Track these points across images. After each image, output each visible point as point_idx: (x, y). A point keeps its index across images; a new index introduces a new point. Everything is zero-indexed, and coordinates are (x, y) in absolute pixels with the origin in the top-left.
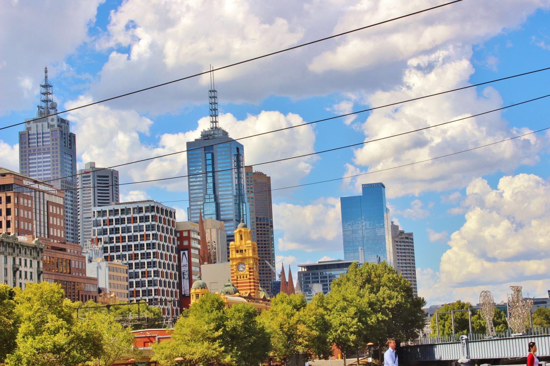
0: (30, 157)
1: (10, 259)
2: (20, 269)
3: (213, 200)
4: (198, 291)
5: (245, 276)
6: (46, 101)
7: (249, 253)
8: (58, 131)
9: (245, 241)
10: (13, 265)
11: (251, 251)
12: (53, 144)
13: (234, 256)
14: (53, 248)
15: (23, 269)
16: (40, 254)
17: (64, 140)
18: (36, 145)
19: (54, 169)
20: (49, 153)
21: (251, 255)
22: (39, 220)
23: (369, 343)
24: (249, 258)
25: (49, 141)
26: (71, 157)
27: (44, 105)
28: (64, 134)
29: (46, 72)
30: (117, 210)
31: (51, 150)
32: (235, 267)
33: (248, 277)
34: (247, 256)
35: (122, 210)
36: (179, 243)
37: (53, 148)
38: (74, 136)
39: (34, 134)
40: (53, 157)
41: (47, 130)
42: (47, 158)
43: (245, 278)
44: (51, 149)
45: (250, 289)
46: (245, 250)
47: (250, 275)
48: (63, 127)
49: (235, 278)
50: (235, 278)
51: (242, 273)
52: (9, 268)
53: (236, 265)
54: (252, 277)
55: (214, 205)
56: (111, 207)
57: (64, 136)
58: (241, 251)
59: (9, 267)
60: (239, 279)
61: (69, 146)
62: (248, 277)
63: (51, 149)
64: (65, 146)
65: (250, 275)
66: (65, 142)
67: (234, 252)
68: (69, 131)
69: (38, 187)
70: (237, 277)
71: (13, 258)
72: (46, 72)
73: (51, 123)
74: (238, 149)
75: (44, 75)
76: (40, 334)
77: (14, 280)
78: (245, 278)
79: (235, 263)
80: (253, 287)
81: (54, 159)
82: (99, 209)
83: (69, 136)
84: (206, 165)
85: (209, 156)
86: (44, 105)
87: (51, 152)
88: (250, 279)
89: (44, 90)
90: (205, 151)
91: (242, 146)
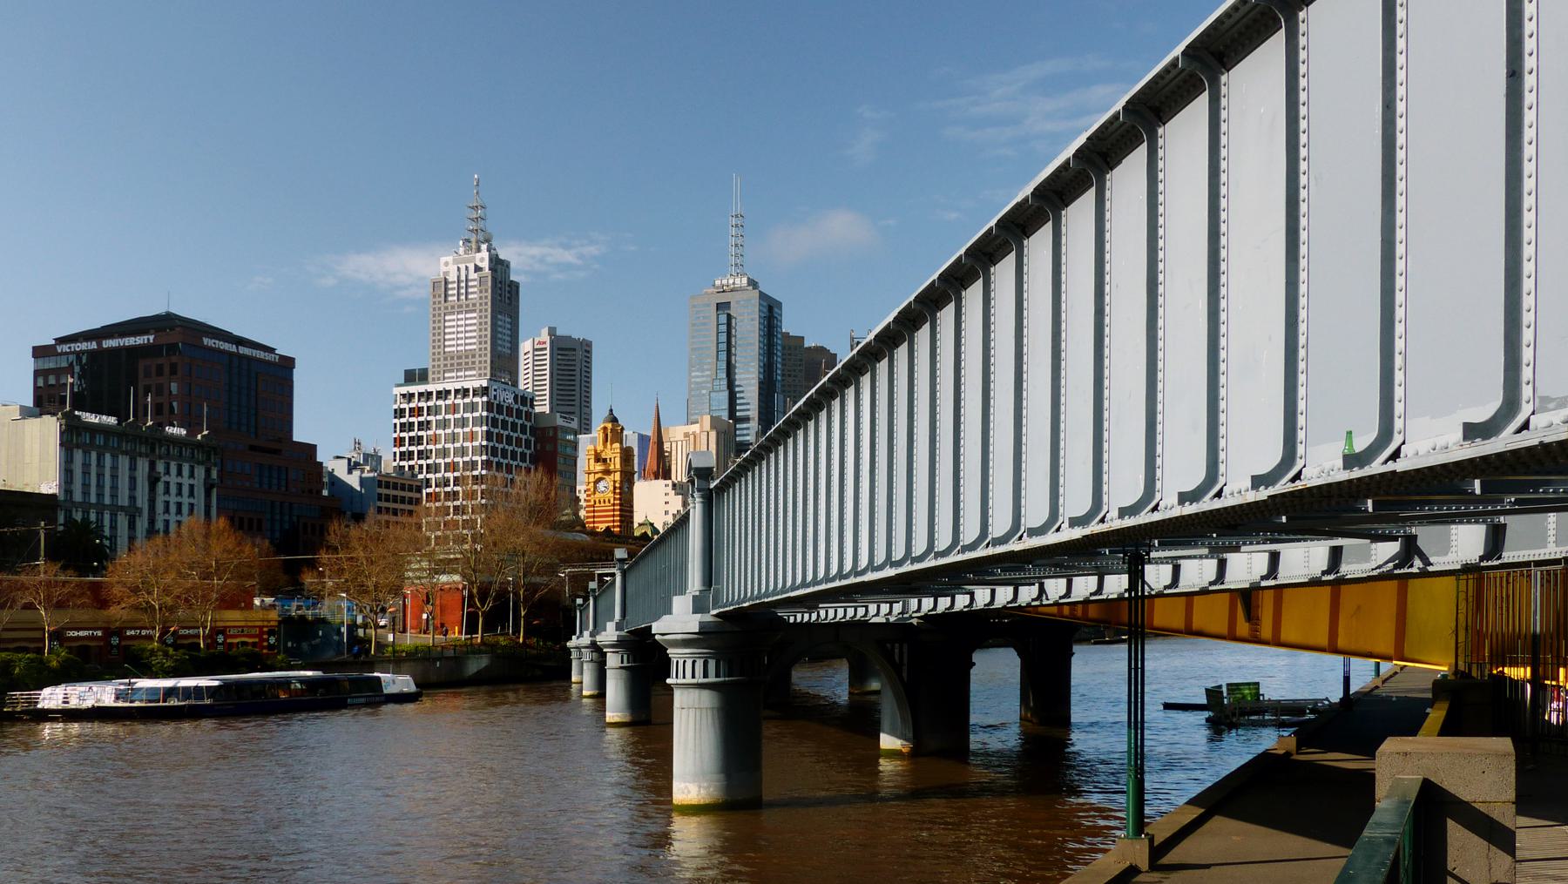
0: (447, 318)
1: (143, 466)
2: (164, 479)
3: (725, 387)
5: (607, 500)
8: (490, 278)
9: (611, 444)
10: (205, 480)
11: (618, 460)
12: (481, 298)
15: (173, 479)
16: (212, 457)
17: (500, 292)
18: (455, 298)
19: (480, 337)
20: (474, 311)
23: (1334, 580)
25: (475, 293)
26: (511, 318)
28: (500, 282)
30: (467, 390)
35: (439, 393)
36: (539, 447)
37: (481, 304)
40: (481, 317)
41: (473, 275)
42: (471, 318)
43: (607, 504)
44: (478, 305)
46: (610, 459)
48: (499, 270)
49: (592, 503)
50: (592, 503)
52: (141, 479)
55: (726, 394)
56: (422, 388)
59: (141, 475)
60: (597, 504)
61: (507, 301)
63: (478, 305)
64: (501, 301)
66: (500, 295)
69: (236, 351)
71: (190, 466)
73: (480, 265)
74: (770, 309)
78: (607, 504)
81: (481, 320)
82: (404, 390)
83: (509, 286)
84: (718, 333)
85: (723, 319)
87: (478, 311)
90: (717, 310)
91: (779, 305)
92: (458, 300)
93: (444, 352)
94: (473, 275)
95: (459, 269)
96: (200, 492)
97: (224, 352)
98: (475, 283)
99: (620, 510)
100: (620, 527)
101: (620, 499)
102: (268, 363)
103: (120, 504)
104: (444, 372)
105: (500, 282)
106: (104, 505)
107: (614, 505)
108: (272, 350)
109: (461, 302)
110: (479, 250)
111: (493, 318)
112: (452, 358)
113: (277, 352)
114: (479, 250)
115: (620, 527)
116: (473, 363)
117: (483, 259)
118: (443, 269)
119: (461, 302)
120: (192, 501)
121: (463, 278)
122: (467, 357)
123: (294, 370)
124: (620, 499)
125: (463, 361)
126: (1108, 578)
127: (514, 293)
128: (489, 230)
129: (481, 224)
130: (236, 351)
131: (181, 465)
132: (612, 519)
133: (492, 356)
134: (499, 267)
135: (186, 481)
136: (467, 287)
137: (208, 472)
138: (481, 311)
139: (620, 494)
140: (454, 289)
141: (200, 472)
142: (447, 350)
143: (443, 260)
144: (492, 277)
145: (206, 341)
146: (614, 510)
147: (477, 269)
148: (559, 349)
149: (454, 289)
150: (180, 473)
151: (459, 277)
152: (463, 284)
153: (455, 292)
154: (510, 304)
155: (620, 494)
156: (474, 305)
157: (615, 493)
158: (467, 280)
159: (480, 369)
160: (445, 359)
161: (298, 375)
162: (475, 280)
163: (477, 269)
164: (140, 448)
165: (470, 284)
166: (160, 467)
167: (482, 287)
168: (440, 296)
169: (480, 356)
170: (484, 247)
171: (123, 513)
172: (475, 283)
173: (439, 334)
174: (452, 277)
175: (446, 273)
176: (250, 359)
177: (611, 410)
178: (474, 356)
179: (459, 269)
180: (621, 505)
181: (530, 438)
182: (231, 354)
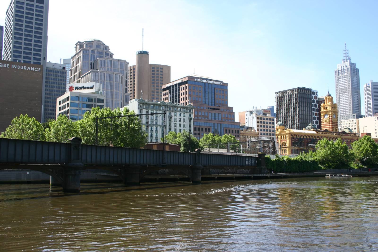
4: (278, 127)
6: (346, 57)
7: (329, 109)
8: (350, 68)
11: (330, 108)
13: (323, 111)
14: (211, 108)
21: (330, 110)
22: (211, 97)
24: (329, 111)
27: (345, 58)
28: (353, 69)
29: (346, 45)
31: (347, 76)
32: (323, 116)
33: (329, 121)
34: (328, 110)
38: (358, 70)
39: (340, 70)
45: (330, 127)
47: (330, 120)
48: (353, 66)
51: (326, 119)
53: (323, 115)
54: (330, 121)
57: (353, 70)
58: (327, 108)
60: (325, 122)
61: (355, 74)
62: (329, 121)
65: (330, 120)
66: (353, 72)
67: (323, 109)
68: (356, 67)
69: (206, 82)
70: (324, 121)
72: (346, 45)
75: (345, 46)
76: (73, 128)
77: (63, 100)
79: (323, 114)
80: (331, 128)
86: (345, 58)
88: (330, 122)
89: (345, 52)
92: (342, 75)
93: (339, 89)
94: (345, 68)
95: (342, 67)
96: (187, 121)
97: (202, 82)
98: (346, 70)
99: (332, 125)
100: (332, 129)
101: (332, 120)
102: (220, 85)
103: (159, 124)
104: (339, 94)
105: (353, 69)
106: (153, 124)
107: (330, 122)
108: (221, 82)
109: (342, 75)
110: (347, 61)
111: (351, 78)
112: (341, 90)
113: (223, 82)
114: (347, 61)
115: (332, 129)
116: (347, 91)
117: (348, 64)
118: (338, 67)
119: (342, 75)
120: (184, 123)
121: (343, 69)
122: (343, 90)
123: (228, 87)
124: (332, 120)
125: (344, 90)
126: (145, 116)
127: (357, 71)
128: (350, 56)
129: (347, 55)
130: (206, 82)
131: (180, 113)
132: (329, 126)
133: (352, 89)
134: (353, 65)
135: (182, 118)
136: (344, 71)
137: (190, 115)
138: (348, 77)
139: (332, 118)
140: (341, 72)
141: (187, 115)
142: (340, 88)
143: (337, 65)
144: (351, 69)
145: (196, 80)
146: (330, 124)
147: (346, 66)
148: (374, 86)
149: (341, 72)
150: (180, 116)
151: (342, 69)
152: (343, 71)
153: (341, 73)
154: (357, 75)
155: (332, 118)
156: (346, 76)
157: (330, 118)
158: (344, 69)
159: (349, 92)
160: (339, 90)
161: (229, 88)
162: (346, 69)
163: (346, 66)
164: (166, 109)
165: (345, 70)
166: (173, 114)
167: (348, 71)
168: (337, 74)
169: (348, 89)
170: (348, 60)
171: (160, 127)
172: (346, 70)
173: (337, 84)
174: (340, 69)
175: (338, 68)
176: (212, 84)
177: (329, 92)
178: (347, 89)
179: (342, 67)
180: (332, 122)
181: (317, 104)
182: (205, 83)
